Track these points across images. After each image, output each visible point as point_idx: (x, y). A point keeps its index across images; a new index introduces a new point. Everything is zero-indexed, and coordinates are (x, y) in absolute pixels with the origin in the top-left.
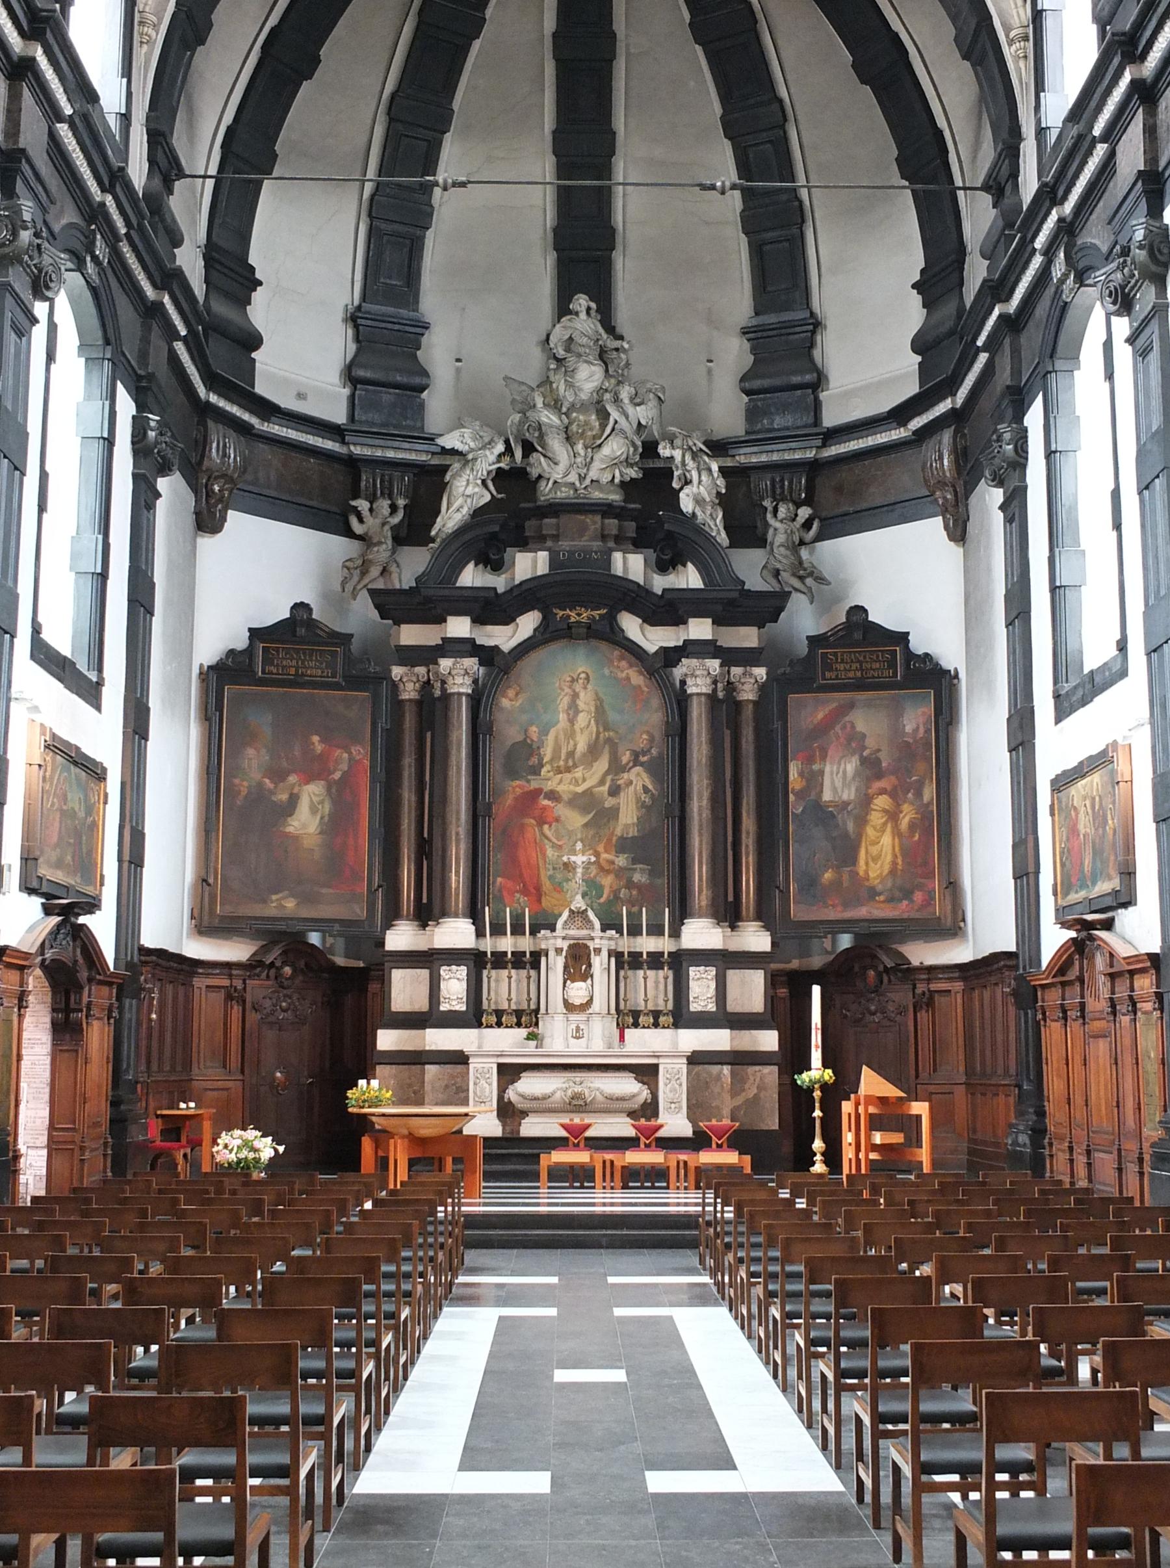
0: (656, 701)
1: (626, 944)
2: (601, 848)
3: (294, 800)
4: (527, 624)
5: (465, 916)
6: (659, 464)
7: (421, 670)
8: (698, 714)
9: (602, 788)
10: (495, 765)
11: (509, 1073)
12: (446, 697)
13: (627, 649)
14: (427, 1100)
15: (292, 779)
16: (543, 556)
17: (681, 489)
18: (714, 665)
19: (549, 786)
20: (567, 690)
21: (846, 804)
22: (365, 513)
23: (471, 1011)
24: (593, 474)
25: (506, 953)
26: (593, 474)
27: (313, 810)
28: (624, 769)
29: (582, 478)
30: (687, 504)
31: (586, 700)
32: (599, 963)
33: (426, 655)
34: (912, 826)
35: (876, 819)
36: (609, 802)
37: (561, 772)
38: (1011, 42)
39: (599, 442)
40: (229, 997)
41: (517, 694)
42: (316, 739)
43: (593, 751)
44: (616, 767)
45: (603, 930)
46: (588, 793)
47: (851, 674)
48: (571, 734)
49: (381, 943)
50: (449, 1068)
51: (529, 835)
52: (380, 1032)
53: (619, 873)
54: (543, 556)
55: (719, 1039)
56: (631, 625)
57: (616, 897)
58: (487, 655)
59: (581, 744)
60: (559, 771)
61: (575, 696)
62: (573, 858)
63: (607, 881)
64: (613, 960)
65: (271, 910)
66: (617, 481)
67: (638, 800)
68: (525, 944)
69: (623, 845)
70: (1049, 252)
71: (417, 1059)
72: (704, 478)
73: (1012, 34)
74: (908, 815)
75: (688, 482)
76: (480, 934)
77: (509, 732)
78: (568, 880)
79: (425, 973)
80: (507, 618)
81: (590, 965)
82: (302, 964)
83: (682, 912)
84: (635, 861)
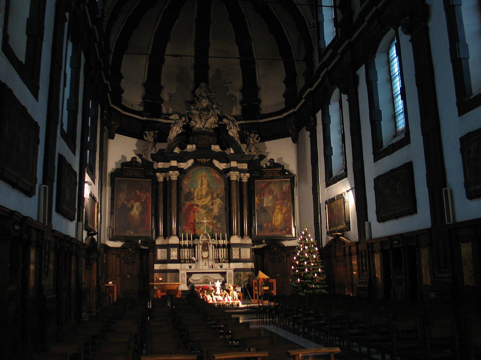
0: (222, 182)
1: (216, 242)
2: (209, 218)
3: (132, 207)
4: (191, 162)
5: (176, 236)
6: (224, 123)
7: (164, 174)
8: (234, 185)
9: (209, 204)
10: (183, 198)
11: (189, 274)
12: (170, 181)
13: (215, 169)
14: (168, 281)
15: (132, 201)
16: (194, 146)
17: (229, 130)
18: (237, 173)
19: (196, 203)
20: (200, 179)
21: (269, 207)
22: (148, 135)
23: (179, 259)
24: (206, 126)
25: (187, 245)
26: (206, 126)
27: (137, 209)
28: (215, 199)
29: (203, 127)
30: (230, 133)
31: (205, 181)
32: (210, 248)
33: (164, 170)
34: (286, 213)
35: (277, 210)
36: (211, 207)
37: (199, 200)
38: (311, 28)
39: (207, 118)
40: (117, 256)
41: (188, 180)
42: (138, 191)
43: (207, 194)
44: (213, 198)
45: (211, 239)
46: (206, 205)
47: (270, 175)
48: (201, 190)
49: (155, 242)
50: (173, 274)
51: (191, 216)
52: (155, 265)
53: (213, 224)
54: (194, 146)
55: (240, 265)
56: (216, 163)
57: (213, 230)
58: (181, 171)
59: (204, 192)
60: (198, 199)
61: (202, 181)
62: (204, 221)
63: (211, 227)
64: (214, 246)
65: (127, 234)
66: (212, 128)
67: (218, 206)
68: (191, 242)
69: (215, 218)
70: (323, 78)
71: (165, 271)
72: (234, 127)
73: (311, 26)
74: (284, 210)
75: (231, 128)
76: (180, 239)
77: (186, 190)
78: (201, 227)
79: (166, 250)
80: (185, 161)
81: (208, 248)
82: (134, 248)
83: (231, 234)
84: (217, 221)
